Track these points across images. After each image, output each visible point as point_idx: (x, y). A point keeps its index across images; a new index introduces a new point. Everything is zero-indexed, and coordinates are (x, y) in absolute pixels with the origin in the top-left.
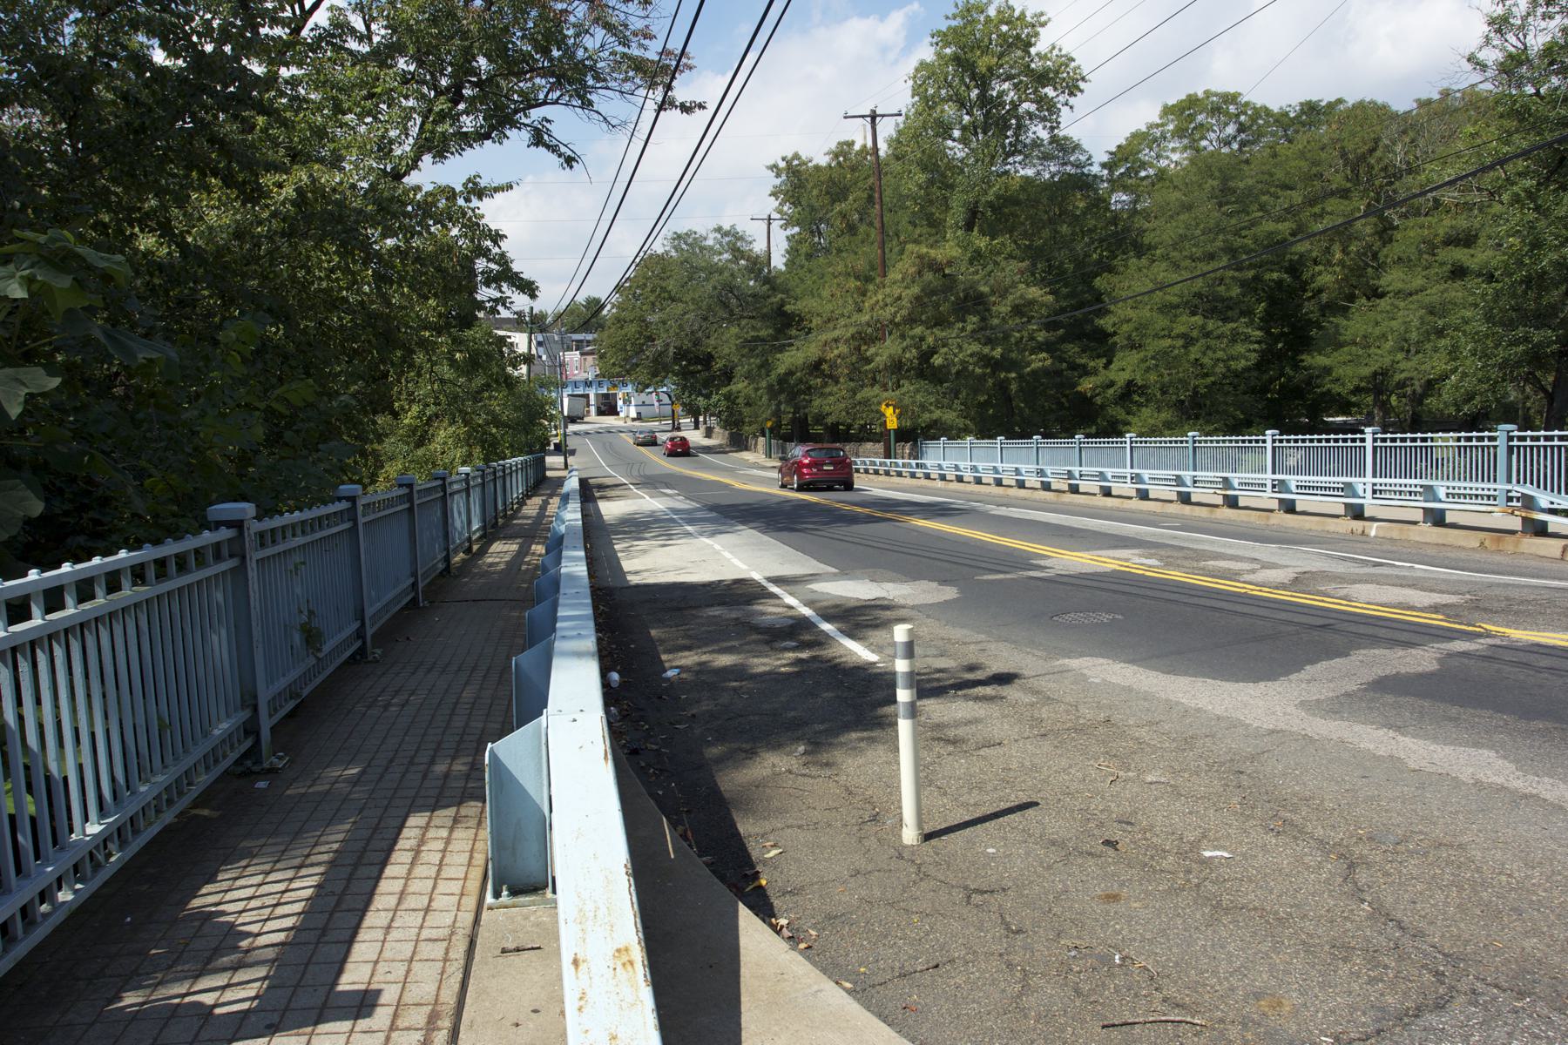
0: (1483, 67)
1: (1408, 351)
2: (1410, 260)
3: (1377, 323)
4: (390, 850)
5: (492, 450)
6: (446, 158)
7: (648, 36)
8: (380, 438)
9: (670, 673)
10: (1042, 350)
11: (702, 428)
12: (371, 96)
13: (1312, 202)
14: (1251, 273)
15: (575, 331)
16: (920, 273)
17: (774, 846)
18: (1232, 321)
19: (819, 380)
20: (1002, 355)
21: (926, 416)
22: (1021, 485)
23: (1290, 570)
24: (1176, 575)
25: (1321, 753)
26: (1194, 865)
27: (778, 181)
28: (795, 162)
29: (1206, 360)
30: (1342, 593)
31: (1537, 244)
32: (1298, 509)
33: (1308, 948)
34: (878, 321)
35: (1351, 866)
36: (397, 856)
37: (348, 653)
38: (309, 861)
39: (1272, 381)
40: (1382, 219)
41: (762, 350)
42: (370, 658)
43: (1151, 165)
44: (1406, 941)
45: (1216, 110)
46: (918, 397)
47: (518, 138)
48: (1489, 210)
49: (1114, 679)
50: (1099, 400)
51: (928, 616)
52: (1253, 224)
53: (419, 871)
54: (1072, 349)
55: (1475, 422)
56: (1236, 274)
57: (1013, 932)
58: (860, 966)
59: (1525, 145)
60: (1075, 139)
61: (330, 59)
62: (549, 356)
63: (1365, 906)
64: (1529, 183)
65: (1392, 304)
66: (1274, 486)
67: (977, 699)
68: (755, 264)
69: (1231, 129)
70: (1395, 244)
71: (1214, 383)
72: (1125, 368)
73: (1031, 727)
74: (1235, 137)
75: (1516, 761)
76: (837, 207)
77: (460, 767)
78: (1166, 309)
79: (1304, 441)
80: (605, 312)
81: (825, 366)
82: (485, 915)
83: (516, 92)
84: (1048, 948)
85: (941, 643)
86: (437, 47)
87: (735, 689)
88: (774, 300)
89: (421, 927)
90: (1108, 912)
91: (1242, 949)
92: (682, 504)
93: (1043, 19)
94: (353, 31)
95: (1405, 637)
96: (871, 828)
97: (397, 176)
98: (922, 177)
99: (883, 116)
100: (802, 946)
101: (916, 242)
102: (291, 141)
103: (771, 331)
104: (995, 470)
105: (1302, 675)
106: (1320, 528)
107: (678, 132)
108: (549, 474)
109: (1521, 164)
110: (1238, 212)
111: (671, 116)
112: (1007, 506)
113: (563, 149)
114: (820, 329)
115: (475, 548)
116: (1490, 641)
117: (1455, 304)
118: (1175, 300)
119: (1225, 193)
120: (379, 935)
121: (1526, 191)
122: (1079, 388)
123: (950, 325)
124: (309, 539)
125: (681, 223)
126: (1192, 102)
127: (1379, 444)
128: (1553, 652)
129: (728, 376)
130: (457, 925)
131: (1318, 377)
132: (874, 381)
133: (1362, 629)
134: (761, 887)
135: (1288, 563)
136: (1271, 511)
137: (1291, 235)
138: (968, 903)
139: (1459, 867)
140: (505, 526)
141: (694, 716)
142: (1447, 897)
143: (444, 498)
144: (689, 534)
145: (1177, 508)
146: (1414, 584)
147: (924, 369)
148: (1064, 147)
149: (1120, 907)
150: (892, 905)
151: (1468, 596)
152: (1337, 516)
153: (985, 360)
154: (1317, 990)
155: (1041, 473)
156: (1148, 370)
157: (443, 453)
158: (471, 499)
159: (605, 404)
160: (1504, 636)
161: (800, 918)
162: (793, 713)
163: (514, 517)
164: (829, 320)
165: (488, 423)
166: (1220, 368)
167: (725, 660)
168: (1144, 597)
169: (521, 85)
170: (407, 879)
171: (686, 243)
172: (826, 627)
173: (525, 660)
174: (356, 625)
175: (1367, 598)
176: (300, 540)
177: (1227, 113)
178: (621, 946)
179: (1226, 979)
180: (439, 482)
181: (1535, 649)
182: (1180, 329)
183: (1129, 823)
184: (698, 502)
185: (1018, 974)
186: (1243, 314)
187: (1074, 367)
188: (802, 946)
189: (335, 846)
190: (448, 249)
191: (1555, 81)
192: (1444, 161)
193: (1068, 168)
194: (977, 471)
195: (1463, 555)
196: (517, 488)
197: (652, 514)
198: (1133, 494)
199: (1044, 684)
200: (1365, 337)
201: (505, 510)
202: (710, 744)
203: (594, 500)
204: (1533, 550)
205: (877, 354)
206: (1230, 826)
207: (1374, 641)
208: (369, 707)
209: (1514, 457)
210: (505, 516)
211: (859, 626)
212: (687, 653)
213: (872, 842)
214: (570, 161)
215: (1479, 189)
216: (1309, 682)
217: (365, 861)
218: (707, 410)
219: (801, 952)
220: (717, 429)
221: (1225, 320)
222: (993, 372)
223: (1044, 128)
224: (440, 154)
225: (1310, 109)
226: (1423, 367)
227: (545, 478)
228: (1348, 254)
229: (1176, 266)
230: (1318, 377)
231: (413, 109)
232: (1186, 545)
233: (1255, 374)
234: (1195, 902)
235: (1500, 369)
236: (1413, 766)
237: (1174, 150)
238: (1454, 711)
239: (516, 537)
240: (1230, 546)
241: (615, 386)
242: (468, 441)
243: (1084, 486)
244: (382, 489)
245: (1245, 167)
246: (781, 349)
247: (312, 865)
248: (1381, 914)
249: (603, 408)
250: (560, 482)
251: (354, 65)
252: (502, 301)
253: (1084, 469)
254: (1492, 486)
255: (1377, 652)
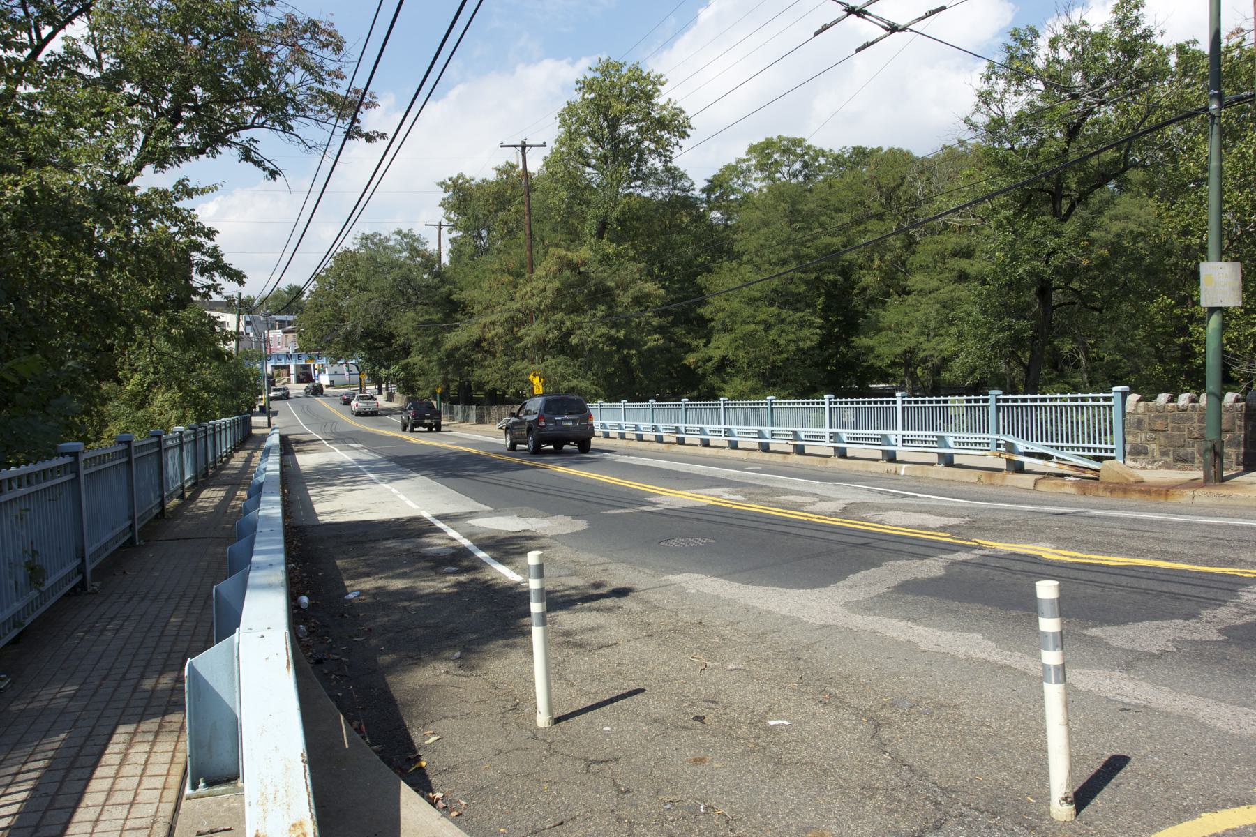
0: (974, 127)
1: (929, 335)
2: (928, 267)
3: (906, 314)
4: (101, 753)
5: (204, 413)
6: (165, 168)
7: (339, 76)
8: (104, 401)
9: (351, 596)
10: (656, 333)
11: (385, 393)
12: (100, 114)
13: (858, 221)
14: (813, 275)
15: (278, 312)
16: (560, 270)
17: (433, 734)
18: (801, 311)
19: (480, 355)
20: (625, 336)
21: (566, 384)
22: (640, 438)
23: (841, 502)
24: (756, 508)
25: (858, 641)
26: (762, 732)
27: (447, 195)
28: (460, 181)
29: (782, 342)
30: (878, 518)
31: (1015, 258)
32: (848, 455)
33: (844, 791)
34: (527, 308)
35: (878, 726)
36: (107, 759)
37: (69, 587)
38: (25, 768)
39: (831, 356)
40: (907, 234)
41: (433, 330)
42: (89, 591)
43: (739, 191)
44: (916, 781)
45: (786, 151)
46: (559, 369)
47: (228, 155)
48: (983, 232)
49: (706, 590)
50: (700, 371)
51: (563, 544)
52: (815, 238)
53: (126, 770)
54: (680, 331)
55: (978, 388)
56: (803, 276)
57: (622, 792)
58: (500, 827)
59: (1005, 185)
60: (682, 170)
61: (63, 81)
62: (255, 334)
63: (887, 756)
64: (1009, 213)
65: (916, 300)
66: (831, 438)
67: (599, 610)
68: (428, 261)
69: (798, 166)
70: (917, 255)
71: (787, 359)
72: (720, 346)
73: (641, 630)
74: (801, 172)
75: (996, 641)
76: (501, 215)
77: (166, 681)
78: (752, 301)
79: (852, 403)
80: (304, 298)
81: (484, 344)
82: (184, 804)
83: (227, 116)
84: (649, 804)
85: (572, 565)
86: (159, 77)
87: (405, 608)
88: (443, 290)
89: (127, 818)
90: (696, 772)
91: (796, 795)
92: (366, 456)
93: (662, 80)
94: (85, 59)
95: (921, 550)
96: (512, 716)
97: (122, 181)
98: (564, 194)
99: (531, 146)
100: (454, 814)
101: (557, 246)
102: (27, 149)
103: (440, 315)
104: (620, 427)
105: (847, 582)
106: (864, 469)
107: (361, 155)
108: (254, 431)
109: (1003, 199)
110: (804, 228)
111: (357, 146)
112: (629, 455)
113: (267, 164)
114: (479, 313)
115: (187, 494)
116: (981, 552)
117: (960, 300)
118: (758, 294)
119: (793, 214)
120: (88, 827)
121: (1006, 218)
122: (685, 362)
123: (584, 312)
124: (34, 489)
125: (364, 226)
126: (769, 143)
127: (906, 405)
128: (1024, 558)
129: (406, 351)
130: (159, 814)
131: (864, 354)
132: (524, 357)
133: (891, 546)
134: (421, 768)
135: (839, 496)
136: (829, 456)
137: (843, 246)
138: (588, 771)
139: (954, 722)
140: (214, 475)
141: (370, 630)
142: (945, 745)
143: (160, 452)
144: (371, 481)
145: (759, 455)
146: (931, 511)
147: (563, 346)
148: (674, 175)
149: (705, 768)
150: (527, 776)
151: (967, 519)
152: (877, 460)
153: (611, 340)
154: (850, 822)
155: (655, 429)
156: (737, 348)
157: (160, 415)
158: (185, 453)
159: (303, 374)
160: (991, 548)
161: (453, 792)
162: (452, 625)
163: (222, 468)
164: (488, 307)
165: (200, 389)
166: (792, 347)
167: (398, 584)
168: (731, 525)
169: (232, 110)
170: (115, 778)
171: (372, 243)
172: (482, 555)
173: (225, 587)
174: (78, 561)
175: (896, 522)
176: (25, 490)
177: (795, 154)
178: (297, 822)
179: (784, 819)
180: (155, 439)
181: (1013, 557)
182: (761, 317)
183: (713, 702)
184: (380, 454)
185: (625, 826)
186: (808, 306)
187: (683, 345)
188: (454, 814)
189: (50, 754)
190: (169, 242)
191: (1024, 139)
192: (950, 195)
193: (676, 192)
194: (605, 428)
195: (965, 488)
196: (226, 443)
197: (341, 464)
198: (726, 444)
199: (653, 596)
200: (897, 324)
201: (215, 462)
202: (382, 653)
203: (292, 453)
204: (1014, 483)
205: (526, 335)
206: (790, 700)
207: (900, 554)
208: (86, 632)
209: (1001, 414)
210: (215, 467)
211: (507, 553)
212: (366, 579)
213: (512, 727)
214: (273, 174)
215: (974, 216)
216: (851, 587)
217: (77, 765)
218: (387, 378)
219: (453, 820)
220: (397, 395)
221: (796, 310)
222: (618, 350)
223: (660, 161)
224: (161, 165)
225: (860, 153)
226: (940, 347)
227: (250, 435)
228: (884, 262)
229: (758, 268)
230: (864, 354)
231: (136, 126)
232: (764, 484)
233: (817, 351)
234: (762, 761)
235: (992, 349)
236: (924, 647)
237: (756, 180)
238: (954, 605)
239: (224, 485)
240: (798, 484)
241: (312, 359)
242: (182, 404)
243: (689, 439)
244: (106, 444)
245: (808, 194)
246: (450, 330)
247: (29, 771)
248: (898, 761)
249: (302, 377)
250: (264, 438)
251: (85, 87)
252: (215, 288)
253: (689, 426)
254: (986, 436)
255: (901, 562)
